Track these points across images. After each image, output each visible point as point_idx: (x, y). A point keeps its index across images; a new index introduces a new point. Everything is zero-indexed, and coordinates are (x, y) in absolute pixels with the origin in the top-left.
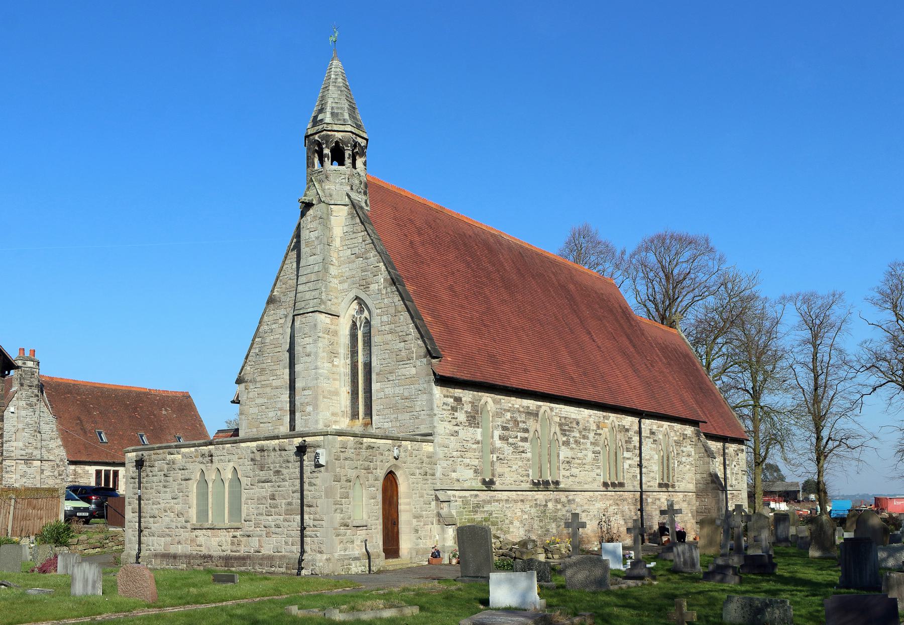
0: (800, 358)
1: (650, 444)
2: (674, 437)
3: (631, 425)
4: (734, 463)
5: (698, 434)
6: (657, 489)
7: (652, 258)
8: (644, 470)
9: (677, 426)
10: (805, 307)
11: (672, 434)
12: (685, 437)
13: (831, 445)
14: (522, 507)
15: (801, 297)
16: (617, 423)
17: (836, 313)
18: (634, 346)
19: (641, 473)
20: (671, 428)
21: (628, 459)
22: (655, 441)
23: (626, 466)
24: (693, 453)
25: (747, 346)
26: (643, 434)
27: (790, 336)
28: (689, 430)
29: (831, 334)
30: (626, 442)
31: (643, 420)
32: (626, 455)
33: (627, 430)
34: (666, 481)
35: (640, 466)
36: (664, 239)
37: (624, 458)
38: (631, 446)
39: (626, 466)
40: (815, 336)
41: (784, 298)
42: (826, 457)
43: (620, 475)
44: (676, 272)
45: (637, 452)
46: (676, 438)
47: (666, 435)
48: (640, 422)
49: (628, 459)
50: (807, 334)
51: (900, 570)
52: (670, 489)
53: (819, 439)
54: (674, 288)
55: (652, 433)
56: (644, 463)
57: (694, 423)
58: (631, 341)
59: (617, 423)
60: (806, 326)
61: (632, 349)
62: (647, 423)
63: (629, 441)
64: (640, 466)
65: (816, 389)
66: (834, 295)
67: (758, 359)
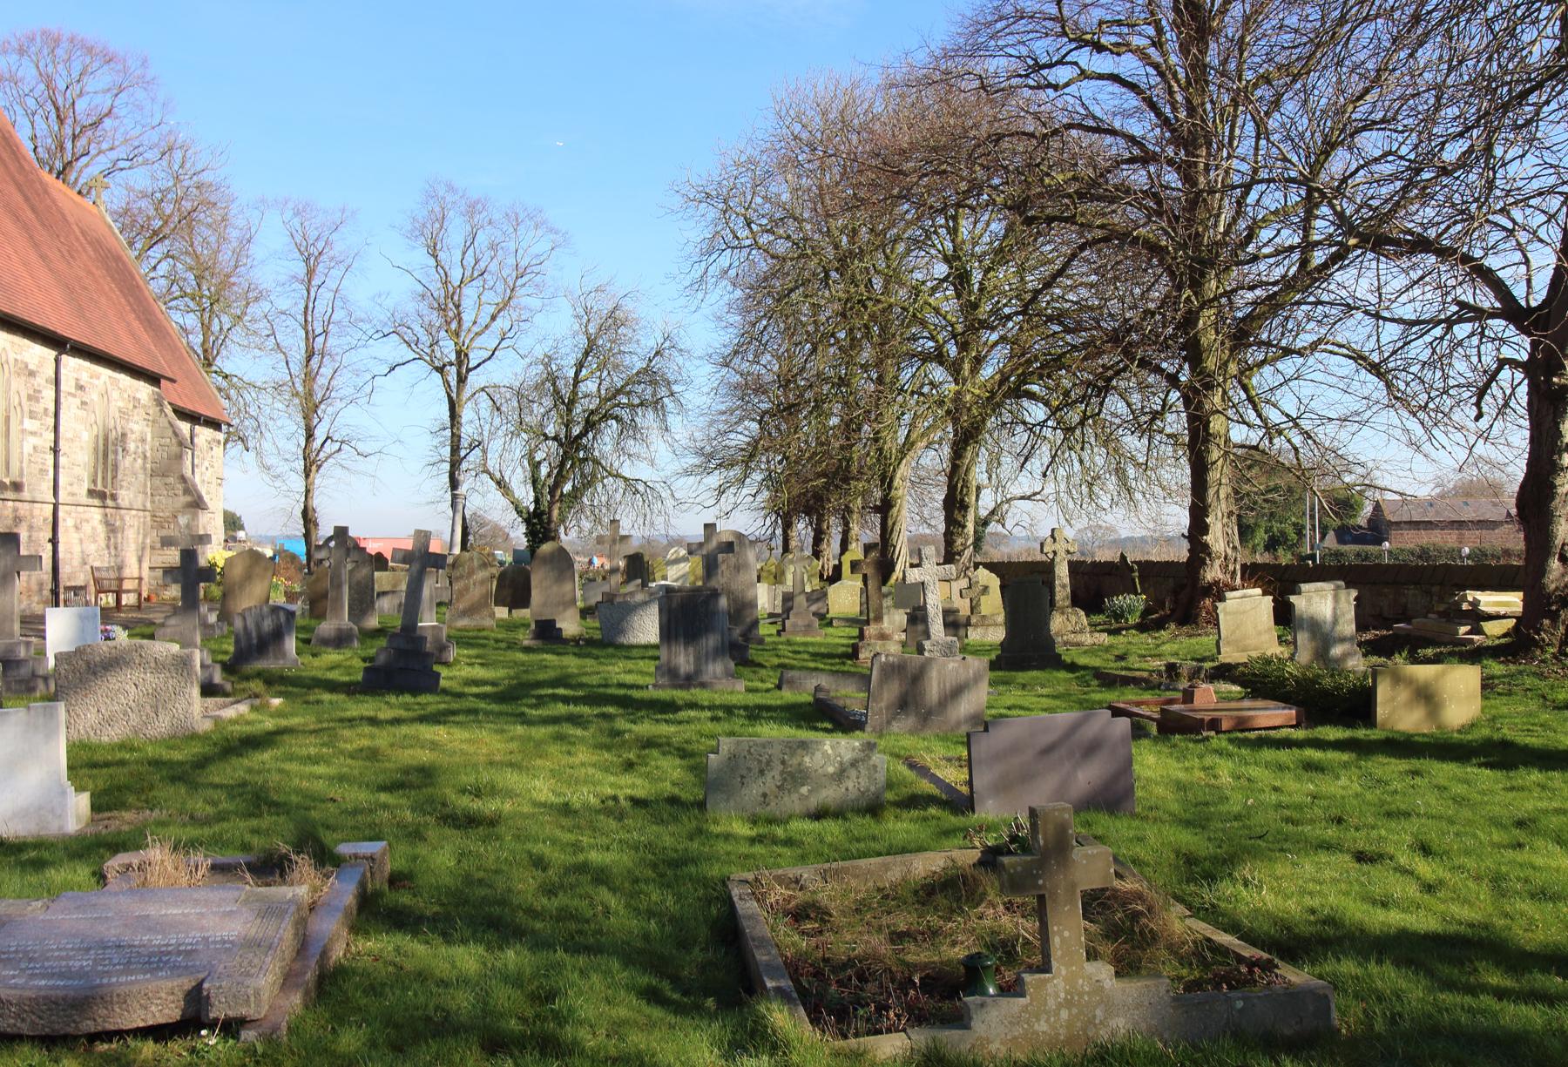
0: (283, 304)
1: (74, 410)
2: (118, 402)
3: (41, 365)
4: (206, 464)
5: (159, 402)
6: (85, 500)
7: (28, 72)
8: (62, 460)
9: (124, 379)
10: (296, 222)
11: (115, 394)
12: (136, 402)
13: (330, 447)
14: (908, 743)
15: (291, 205)
16: (12, 356)
17: (342, 244)
18: (33, 210)
19: (56, 466)
20: (115, 382)
21: (33, 433)
22: (84, 403)
23: (28, 449)
24: (149, 438)
25: (202, 271)
26: (63, 387)
27: (270, 266)
28: (144, 390)
29: (336, 273)
30: (30, 398)
31: (64, 358)
32: (29, 424)
33: (32, 374)
34: (99, 487)
35: (55, 451)
36: (57, 41)
37: (23, 431)
38: (39, 408)
39: (28, 449)
40: (310, 273)
41: (263, 201)
42: (319, 467)
43: (15, 466)
44: (81, 105)
45: (51, 421)
46: (121, 404)
47: (105, 394)
48: (57, 361)
49: (33, 433)
50: (301, 269)
51: (1567, 841)
52: (109, 502)
53: (310, 436)
54: (75, 137)
55: (81, 388)
56: (62, 445)
57: (153, 379)
58: (27, 199)
59: (12, 356)
60: (297, 255)
61: (29, 213)
62: (71, 363)
63: (34, 397)
64: (55, 451)
65: (309, 359)
66: (343, 211)
67: (215, 291)
